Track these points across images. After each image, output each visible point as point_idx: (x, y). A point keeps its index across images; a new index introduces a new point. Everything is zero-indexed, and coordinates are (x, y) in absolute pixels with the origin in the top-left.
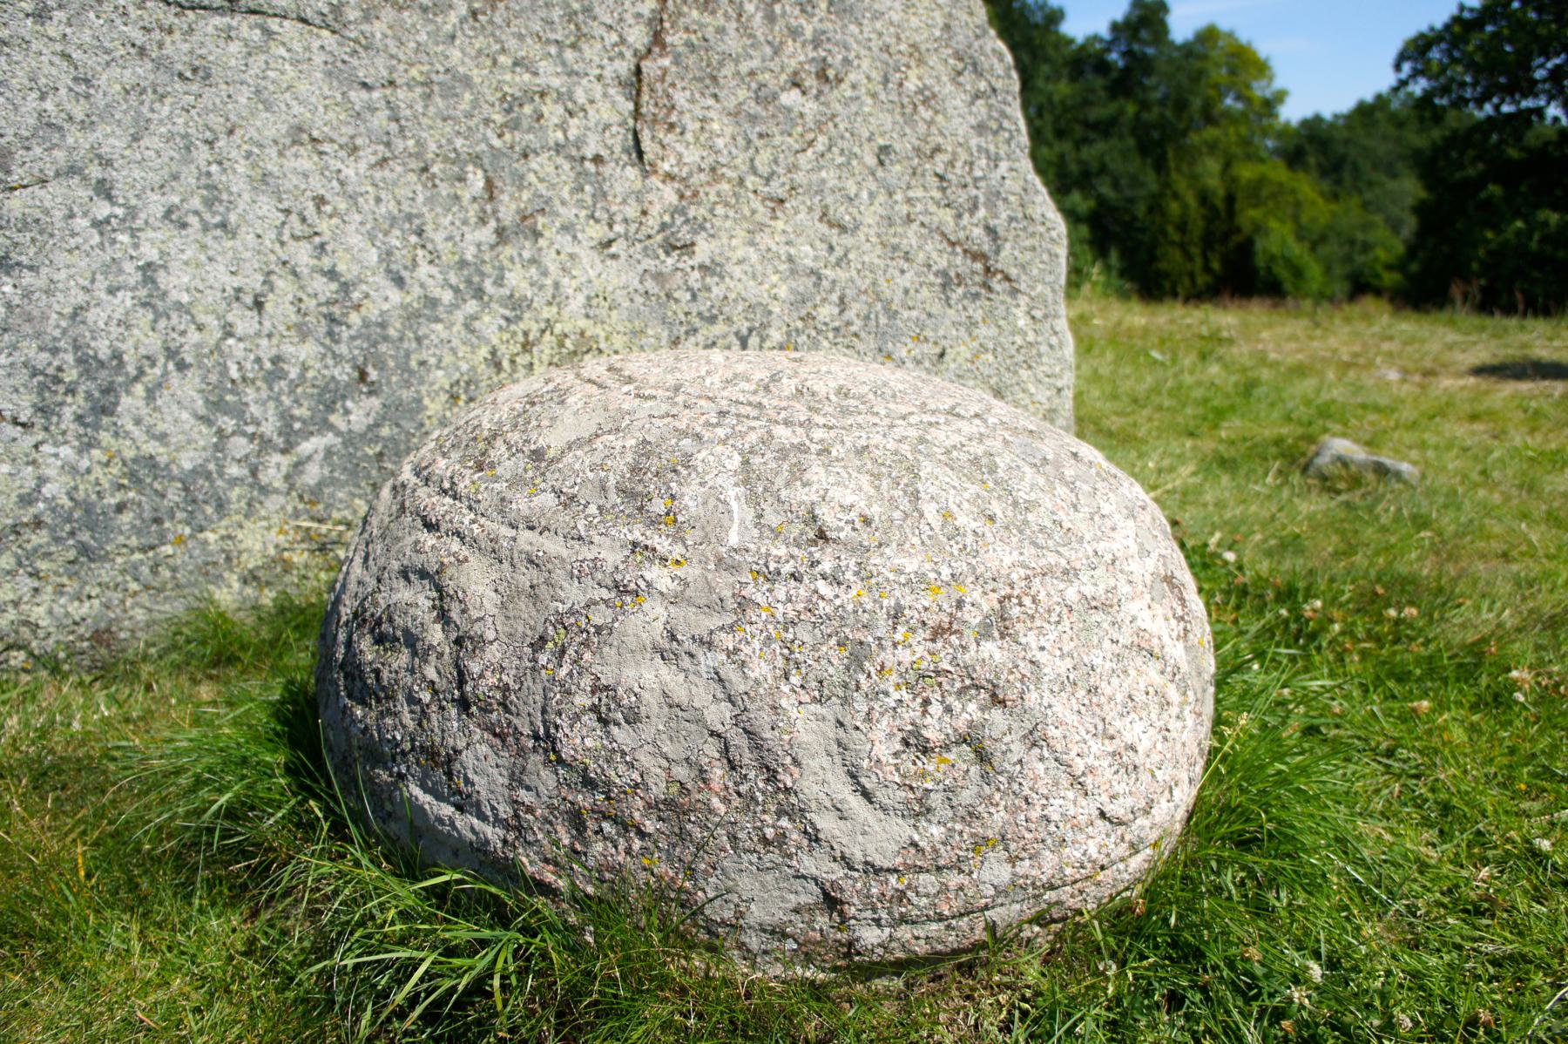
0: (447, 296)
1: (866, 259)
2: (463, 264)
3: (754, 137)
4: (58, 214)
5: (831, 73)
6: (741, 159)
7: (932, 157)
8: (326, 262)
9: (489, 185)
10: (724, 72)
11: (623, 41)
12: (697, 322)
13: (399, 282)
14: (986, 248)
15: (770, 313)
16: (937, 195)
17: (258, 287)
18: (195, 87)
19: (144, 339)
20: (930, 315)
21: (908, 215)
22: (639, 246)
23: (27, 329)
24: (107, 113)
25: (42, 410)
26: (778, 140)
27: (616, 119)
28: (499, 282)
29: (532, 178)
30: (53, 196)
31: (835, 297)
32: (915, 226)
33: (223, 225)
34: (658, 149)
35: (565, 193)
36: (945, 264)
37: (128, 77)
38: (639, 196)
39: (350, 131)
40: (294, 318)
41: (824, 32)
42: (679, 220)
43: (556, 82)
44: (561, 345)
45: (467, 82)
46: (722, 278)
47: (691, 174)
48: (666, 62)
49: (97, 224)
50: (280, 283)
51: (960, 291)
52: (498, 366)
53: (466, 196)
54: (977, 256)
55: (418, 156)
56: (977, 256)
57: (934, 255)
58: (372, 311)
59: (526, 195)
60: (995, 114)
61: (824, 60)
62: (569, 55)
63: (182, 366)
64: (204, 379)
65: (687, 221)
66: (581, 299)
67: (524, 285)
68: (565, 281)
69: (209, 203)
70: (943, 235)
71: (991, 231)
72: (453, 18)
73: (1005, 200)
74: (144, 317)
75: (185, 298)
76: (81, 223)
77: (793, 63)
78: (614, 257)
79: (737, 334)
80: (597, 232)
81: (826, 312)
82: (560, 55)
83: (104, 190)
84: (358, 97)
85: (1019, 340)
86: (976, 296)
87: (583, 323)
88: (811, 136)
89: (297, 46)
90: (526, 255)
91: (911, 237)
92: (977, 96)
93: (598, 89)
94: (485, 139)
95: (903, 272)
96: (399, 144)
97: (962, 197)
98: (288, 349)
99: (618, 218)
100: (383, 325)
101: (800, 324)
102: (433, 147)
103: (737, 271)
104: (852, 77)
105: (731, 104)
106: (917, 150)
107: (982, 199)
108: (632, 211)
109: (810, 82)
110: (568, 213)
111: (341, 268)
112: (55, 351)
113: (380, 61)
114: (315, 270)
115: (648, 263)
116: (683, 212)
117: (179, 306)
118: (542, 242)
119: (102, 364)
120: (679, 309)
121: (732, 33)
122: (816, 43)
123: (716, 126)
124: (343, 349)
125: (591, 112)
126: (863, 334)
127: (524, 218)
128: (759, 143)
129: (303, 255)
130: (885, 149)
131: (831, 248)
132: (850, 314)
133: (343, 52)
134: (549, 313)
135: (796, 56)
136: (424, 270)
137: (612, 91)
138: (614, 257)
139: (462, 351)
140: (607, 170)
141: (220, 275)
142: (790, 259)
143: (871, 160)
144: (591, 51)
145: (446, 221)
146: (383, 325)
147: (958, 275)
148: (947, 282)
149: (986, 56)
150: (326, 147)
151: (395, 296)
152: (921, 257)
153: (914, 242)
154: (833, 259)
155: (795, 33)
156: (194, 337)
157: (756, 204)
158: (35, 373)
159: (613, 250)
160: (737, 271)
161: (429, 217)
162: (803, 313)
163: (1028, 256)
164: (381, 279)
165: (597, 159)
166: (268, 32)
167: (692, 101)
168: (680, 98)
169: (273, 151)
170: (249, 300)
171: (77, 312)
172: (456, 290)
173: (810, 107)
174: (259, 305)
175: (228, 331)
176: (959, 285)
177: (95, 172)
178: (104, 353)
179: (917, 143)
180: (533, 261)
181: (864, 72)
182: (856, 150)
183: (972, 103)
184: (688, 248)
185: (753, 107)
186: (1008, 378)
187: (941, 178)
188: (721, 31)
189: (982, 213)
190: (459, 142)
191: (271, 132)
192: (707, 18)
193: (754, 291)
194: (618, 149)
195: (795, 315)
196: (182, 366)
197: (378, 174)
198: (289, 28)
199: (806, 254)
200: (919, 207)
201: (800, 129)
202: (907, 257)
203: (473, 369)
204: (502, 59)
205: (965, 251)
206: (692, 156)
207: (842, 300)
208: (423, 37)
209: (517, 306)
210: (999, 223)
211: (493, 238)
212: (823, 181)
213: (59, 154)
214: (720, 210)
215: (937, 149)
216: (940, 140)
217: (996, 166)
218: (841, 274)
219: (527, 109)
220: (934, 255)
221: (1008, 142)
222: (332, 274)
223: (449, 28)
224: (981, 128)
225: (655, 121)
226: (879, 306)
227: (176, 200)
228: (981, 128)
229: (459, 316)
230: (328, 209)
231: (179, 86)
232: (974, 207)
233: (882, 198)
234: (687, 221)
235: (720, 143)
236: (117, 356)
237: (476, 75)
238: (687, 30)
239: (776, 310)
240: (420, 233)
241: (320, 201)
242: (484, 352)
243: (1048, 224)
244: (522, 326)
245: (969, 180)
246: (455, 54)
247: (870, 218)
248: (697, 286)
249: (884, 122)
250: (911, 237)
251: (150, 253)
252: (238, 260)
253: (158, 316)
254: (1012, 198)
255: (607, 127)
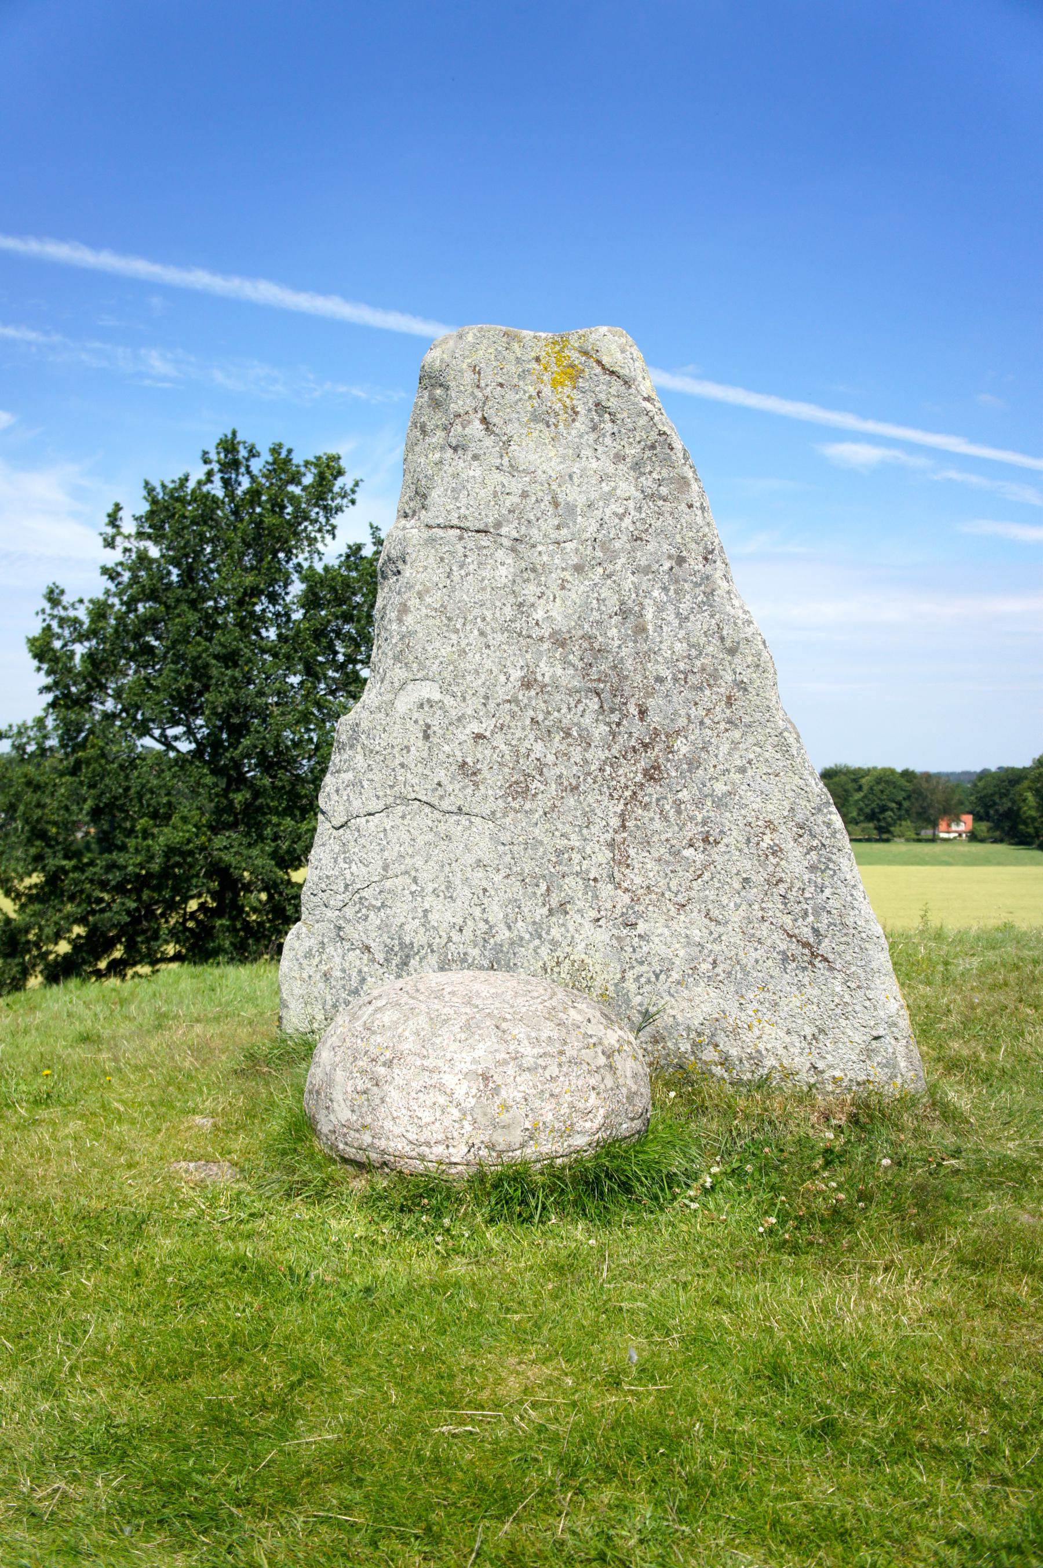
0: (527, 936)
1: (732, 940)
2: (534, 923)
3: (669, 872)
4: (400, 888)
5: (711, 839)
6: (663, 883)
7: (777, 884)
8: (485, 916)
9: (548, 889)
10: (654, 839)
11: (608, 825)
12: (635, 964)
13: (509, 928)
14: (811, 940)
15: (673, 963)
16: (782, 907)
17: (461, 923)
18: (446, 843)
19: (421, 939)
20: (772, 977)
21: (763, 917)
22: (611, 923)
23: (385, 929)
24: (418, 852)
25: (386, 960)
26: (681, 874)
27: (605, 861)
28: (548, 933)
29: (566, 887)
30: (399, 881)
31: (710, 960)
32: (767, 924)
33: (451, 897)
34: (621, 876)
35: (580, 895)
36: (785, 947)
37: (427, 838)
38: (612, 898)
39: (496, 862)
40: (472, 938)
41: (709, 817)
42: (631, 912)
43: (577, 844)
44: (573, 965)
45: (541, 843)
46: (648, 942)
47: (637, 889)
48: (625, 835)
49: (412, 893)
50: (469, 923)
51: (794, 965)
52: (546, 970)
53: (539, 893)
54: (806, 945)
55: (521, 874)
56: (806, 945)
57: (778, 942)
58: (498, 939)
59: (563, 894)
60: (824, 860)
61: (708, 832)
62: (585, 831)
63: (432, 951)
64: (439, 958)
65: (634, 913)
66: (583, 944)
67: (559, 935)
68: (577, 936)
69: (447, 888)
70: (785, 930)
71: (816, 931)
72: (537, 816)
73: (829, 912)
74: (422, 930)
75: (436, 925)
76: (407, 892)
77: (690, 834)
78: (600, 926)
79: (654, 972)
80: (594, 914)
81: (705, 967)
82: (580, 831)
83: (415, 880)
84: (501, 848)
85: (837, 1000)
86: (804, 969)
87: (583, 956)
88: (700, 872)
89: (480, 828)
90: (561, 922)
91: (764, 930)
92: (812, 849)
93: (597, 846)
94: (548, 868)
95: (756, 949)
96: (515, 869)
97: (797, 909)
98: (470, 950)
99: (602, 908)
100: (501, 945)
101: (690, 972)
102: (527, 871)
103: (656, 940)
104: (725, 841)
105: (656, 855)
106: (767, 881)
107: (810, 911)
108: (609, 906)
109: (699, 844)
110: (580, 904)
111: (490, 919)
112: (392, 939)
113: (508, 834)
114: (481, 919)
115: (615, 931)
116: (632, 908)
117: (434, 927)
118: (568, 917)
119: (406, 946)
120: (627, 955)
121: (657, 820)
122: (704, 823)
123: (649, 866)
124: (487, 953)
125: (594, 857)
126: (726, 982)
127: (561, 905)
128: (672, 875)
129: (477, 912)
130: (746, 880)
131: (711, 933)
132: (719, 970)
133: (496, 830)
134: (568, 949)
135: (692, 830)
136: (520, 924)
137: (603, 848)
138: (600, 926)
139: (532, 961)
140: (599, 885)
141: (448, 917)
142: (687, 936)
143: (737, 886)
144: (594, 829)
145: (529, 904)
146: (501, 945)
147: (793, 955)
148: (786, 958)
149: (818, 826)
150: (488, 869)
151: (507, 934)
152: (769, 942)
153: (765, 933)
154: (711, 939)
155: (691, 818)
156: (437, 940)
157: (670, 906)
158: (386, 946)
159: (600, 923)
160: (656, 940)
161: (523, 901)
162: (692, 966)
163: (843, 947)
164: (502, 926)
165: (595, 880)
166: (471, 822)
167: (637, 854)
168: (632, 852)
169: (470, 869)
170: (457, 928)
171: (403, 924)
172: (531, 934)
173: (700, 857)
174: (461, 930)
175: (450, 939)
176: (794, 961)
177: (413, 873)
178: (408, 942)
179: (767, 877)
180: (563, 925)
181: (734, 837)
182: (728, 880)
183: (808, 853)
184: (634, 925)
185: (667, 857)
186: (830, 1023)
187: (784, 897)
188: (652, 819)
189: (811, 919)
190: (537, 869)
191: (470, 862)
192: (646, 814)
193: (663, 950)
194: (604, 875)
195: (688, 966)
196: (432, 951)
197: (506, 881)
198: (477, 820)
199: (696, 935)
200: (771, 913)
201: (693, 869)
202: (759, 941)
203: (536, 970)
204: (557, 833)
205: (798, 941)
206: (638, 880)
207: (715, 962)
208: (524, 824)
209: (555, 944)
210: (822, 927)
211: (547, 913)
212: (707, 896)
213: (403, 866)
214: (650, 908)
215: (781, 880)
216: (783, 875)
217: (822, 891)
218: (716, 948)
219: (566, 856)
220: (778, 942)
221: (832, 876)
222: (486, 921)
223: (535, 820)
224: (812, 868)
225: (620, 863)
226: (738, 968)
227: (437, 886)
228: (812, 868)
229: (531, 946)
230: (487, 894)
231: (442, 842)
232: (806, 913)
233: (744, 907)
234: (634, 913)
235: (651, 874)
236: (412, 944)
237: (545, 840)
238: (636, 819)
239: (677, 963)
240: (519, 908)
241: (485, 890)
242: (541, 963)
243: (860, 929)
244: (557, 954)
245: (802, 899)
246: (537, 831)
247: (736, 918)
248: (636, 945)
249: (746, 866)
250: (764, 930)
251: (427, 906)
252: (455, 912)
253: (427, 930)
254: (834, 911)
255: (600, 865)
